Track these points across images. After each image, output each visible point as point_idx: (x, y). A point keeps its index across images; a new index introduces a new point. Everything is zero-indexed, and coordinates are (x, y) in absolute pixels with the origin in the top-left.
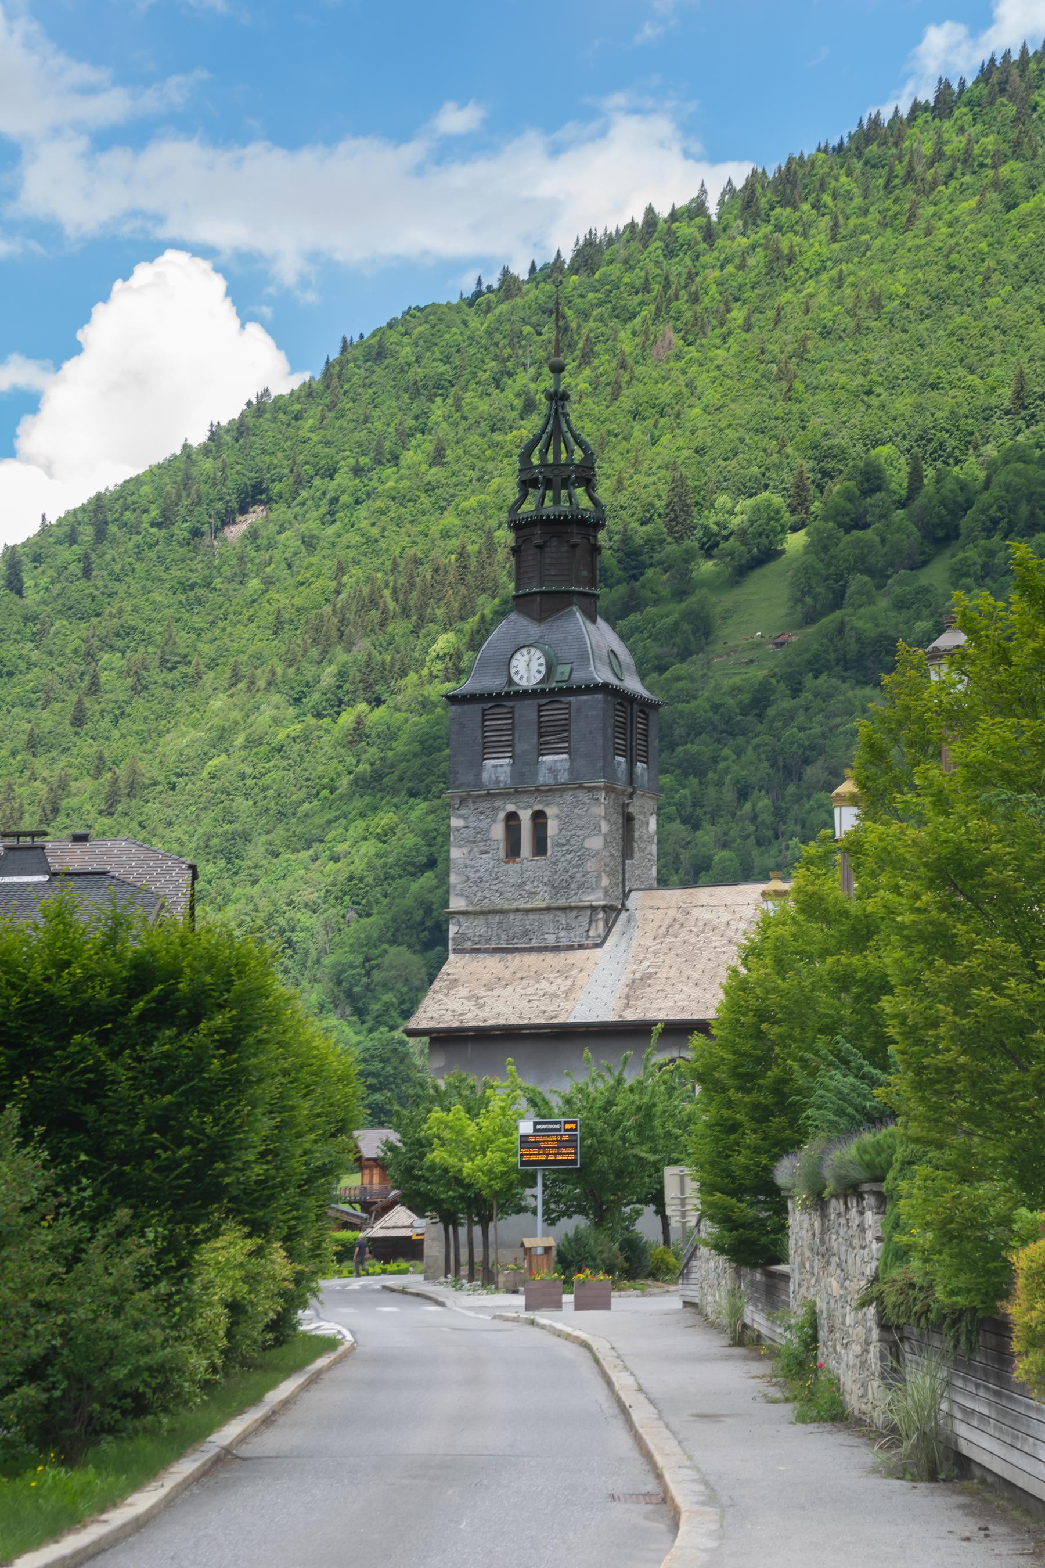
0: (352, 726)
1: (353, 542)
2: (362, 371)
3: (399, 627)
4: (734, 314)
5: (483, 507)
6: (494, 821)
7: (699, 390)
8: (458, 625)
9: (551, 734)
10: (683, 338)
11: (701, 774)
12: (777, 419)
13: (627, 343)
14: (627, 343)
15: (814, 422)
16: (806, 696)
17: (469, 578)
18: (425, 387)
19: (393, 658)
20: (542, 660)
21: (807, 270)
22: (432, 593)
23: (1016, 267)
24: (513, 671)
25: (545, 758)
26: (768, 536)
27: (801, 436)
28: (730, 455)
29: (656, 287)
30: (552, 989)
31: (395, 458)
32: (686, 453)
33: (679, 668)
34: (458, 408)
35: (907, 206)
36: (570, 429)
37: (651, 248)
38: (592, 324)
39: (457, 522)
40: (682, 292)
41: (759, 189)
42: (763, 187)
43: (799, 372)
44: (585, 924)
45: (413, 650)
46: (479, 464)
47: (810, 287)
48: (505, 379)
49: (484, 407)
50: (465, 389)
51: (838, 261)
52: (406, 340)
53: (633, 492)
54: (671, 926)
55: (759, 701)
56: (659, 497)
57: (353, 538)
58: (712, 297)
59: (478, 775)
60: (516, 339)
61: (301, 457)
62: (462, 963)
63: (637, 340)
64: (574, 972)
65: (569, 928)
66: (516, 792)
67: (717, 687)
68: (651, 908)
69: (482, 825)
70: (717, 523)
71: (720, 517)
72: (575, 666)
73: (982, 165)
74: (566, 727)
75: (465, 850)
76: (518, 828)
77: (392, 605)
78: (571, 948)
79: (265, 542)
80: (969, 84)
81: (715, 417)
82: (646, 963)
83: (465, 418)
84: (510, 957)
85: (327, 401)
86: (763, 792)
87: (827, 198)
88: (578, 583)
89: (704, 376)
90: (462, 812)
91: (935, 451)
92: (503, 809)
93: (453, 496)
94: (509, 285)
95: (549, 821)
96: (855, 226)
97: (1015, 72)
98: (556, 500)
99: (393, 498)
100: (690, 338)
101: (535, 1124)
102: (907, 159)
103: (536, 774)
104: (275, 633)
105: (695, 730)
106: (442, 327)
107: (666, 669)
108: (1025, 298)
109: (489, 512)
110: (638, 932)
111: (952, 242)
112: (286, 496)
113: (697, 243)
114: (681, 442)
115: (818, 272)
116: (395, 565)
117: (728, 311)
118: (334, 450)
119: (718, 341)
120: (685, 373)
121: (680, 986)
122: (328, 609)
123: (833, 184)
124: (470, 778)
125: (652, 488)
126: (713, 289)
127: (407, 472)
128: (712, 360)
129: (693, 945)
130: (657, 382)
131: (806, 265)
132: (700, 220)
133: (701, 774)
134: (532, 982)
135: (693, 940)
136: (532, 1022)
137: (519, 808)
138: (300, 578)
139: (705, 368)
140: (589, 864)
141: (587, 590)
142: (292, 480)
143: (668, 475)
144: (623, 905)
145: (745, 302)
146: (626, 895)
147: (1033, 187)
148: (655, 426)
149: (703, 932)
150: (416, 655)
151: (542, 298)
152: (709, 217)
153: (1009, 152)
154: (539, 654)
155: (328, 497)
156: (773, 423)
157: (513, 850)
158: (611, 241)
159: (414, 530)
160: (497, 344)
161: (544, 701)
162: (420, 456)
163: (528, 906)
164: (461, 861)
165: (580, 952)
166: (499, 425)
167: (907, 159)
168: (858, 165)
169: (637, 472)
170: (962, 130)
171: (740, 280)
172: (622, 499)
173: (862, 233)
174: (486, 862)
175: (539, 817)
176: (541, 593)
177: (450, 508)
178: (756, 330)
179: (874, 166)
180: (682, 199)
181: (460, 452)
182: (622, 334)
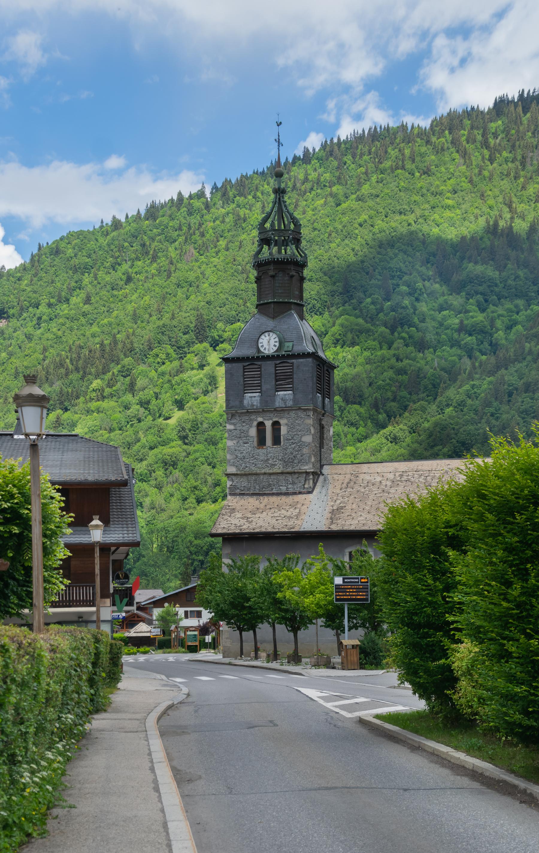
0: (55, 420)
1: (50, 338)
2: (49, 259)
3: (74, 376)
4: (221, 242)
5: (110, 324)
6: (251, 427)
7: (207, 276)
8: (102, 377)
9: (283, 380)
10: (198, 252)
11: (215, 444)
13: (173, 253)
14: (173, 253)
17: (106, 356)
18: (79, 268)
19: (72, 390)
20: (277, 339)
22: (89, 361)
23: (342, 231)
24: (260, 345)
25: (279, 393)
29: (185, 228)
30: (288, 514)
31: (67, 300)
32: (202, 303)
33: (202, 398)
34: (96, 279)
35: (294, 201)
36: (288, 212)
37: (182, 211)
38: (156, 243)
39: (98, 330)
40: (197, 232)
41: (229, 188)
44: (303, 481)
45: (81, 387)
46: (107, 304)
48: (117, 266)
49: (108, 278)
50: (99, 270)
52: (69, 246)
53: (180, 320)
54: (348, 483)
56: (191, 323)
57: (50, 336)
59: (242, 402)
60: (121, 248)
61: (23, 298)
62: (235, 500)
63: (177, 252)
64: (299, 506)
65: (293, 483)
66: (263, 411)
69: (244, 428)
70: (218, 336)
71: (220, 333)
72: (295, 343)
73: (325, 186)
75: (235, 442)
76: (264, 431)
77: (70, 367)
78: (295, 494)
79: (7, 336)
80: (317, 150)
82: (338, 502)
83: (100, 283)
84: (261, 498)
85: (33, 273)
87: (259, 194)
88: (294, 298)
89: (209, 269)
90: (232, 421)
91: (311, 308)
92: (256, 420)
93: (96, 318)
94: (116, 224)
97: (336, 148)
98: (280, 252)
99: (68, 318)
100: (202, 252)
101: (344, 579)
102: (293, 180)
104: (15, 377)
106: (86, 241)
108: (346, 245)
109: (113, 326)
110: (331, 486)
111: (314, 218)
112: (16, 315)
113: (202, 210)
114: (200, 298)
116: (71, 349)
117: (218, 241)
118: (38, 295)
119: (214, 255)
121: (360, 513)
122: (40, 367)
123: (261, 188)
126: (211, 231)
127: (74, 307)
129: (363, 493)
131: (252, 223)
132: (203, 200)
133: (215, 444)
135: (363, 490)
137: (265, 419)
138: (26, 353)
140: (305, 450)
141: (298, 302)
142: (18, 308)
143: (195, 313)
144: (321, 472)
145: (225, 238)
146: (322, 466)
147: (347, 197)
148: (188, 291)
149: (367, 486)
150: (83, 389)
151: (133, 231)
153: (336, 181)
154: (275, 336)
155: (37, 316)
156: (241, 292)
157: (262, 442)
158: (163, 206)
159: (79, 333)
160: (112, 250)
162: (79, 300)
163: (271, 471)
165: (300, 496)
166: (115, 287)
167: (293, 180)
169: (181, 311)
170: (315, 170)
172: (174, 323)
174: (247, 448)
175: (276, 425)
176: (274, 302)
177: (95, 324)
178: (231, 250)
180: (194, 190)
181: (98, 298)
182: (170, 249)
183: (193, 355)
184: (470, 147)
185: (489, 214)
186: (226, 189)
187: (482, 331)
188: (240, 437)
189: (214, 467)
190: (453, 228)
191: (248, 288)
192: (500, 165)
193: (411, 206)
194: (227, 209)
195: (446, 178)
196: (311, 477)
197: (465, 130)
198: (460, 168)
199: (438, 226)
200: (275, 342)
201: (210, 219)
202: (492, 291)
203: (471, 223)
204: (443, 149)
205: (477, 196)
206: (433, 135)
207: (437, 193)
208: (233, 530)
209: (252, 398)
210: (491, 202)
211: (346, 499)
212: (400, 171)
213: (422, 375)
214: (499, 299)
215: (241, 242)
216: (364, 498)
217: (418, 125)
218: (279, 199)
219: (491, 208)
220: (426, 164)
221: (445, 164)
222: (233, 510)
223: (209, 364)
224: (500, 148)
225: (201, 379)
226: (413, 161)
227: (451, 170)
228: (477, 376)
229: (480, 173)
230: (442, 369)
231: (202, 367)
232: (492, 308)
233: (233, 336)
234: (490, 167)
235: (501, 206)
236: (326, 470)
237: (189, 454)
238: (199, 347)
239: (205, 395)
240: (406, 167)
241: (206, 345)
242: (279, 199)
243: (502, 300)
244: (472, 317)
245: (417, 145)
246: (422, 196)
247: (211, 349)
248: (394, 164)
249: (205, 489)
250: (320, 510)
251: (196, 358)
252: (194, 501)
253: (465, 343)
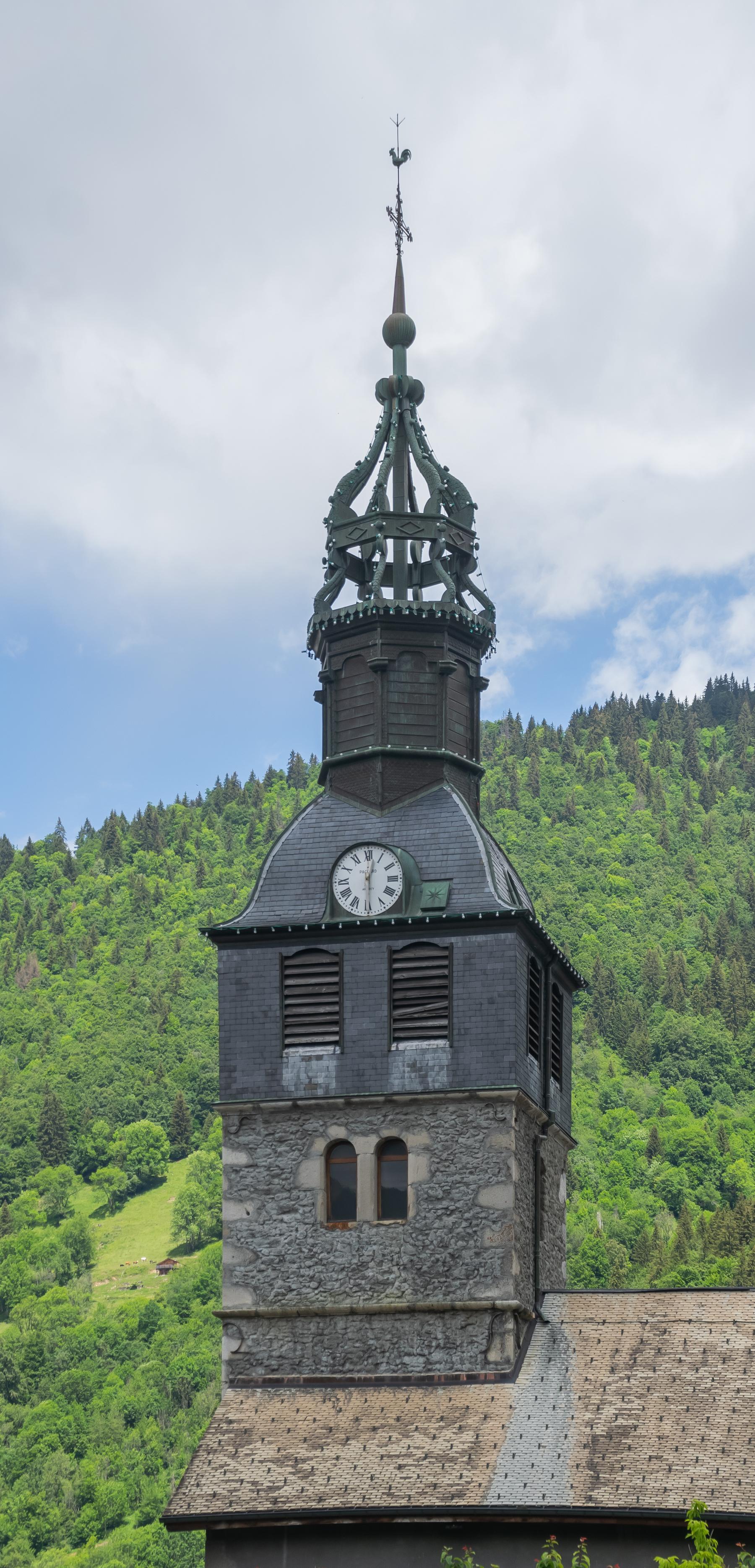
4: (102, 946)
6: (306, 1156)
7: (68, 1017)
9: (419, 1003)
10: (49, 967)
11: (84, 1398)
12: (152, 1049)
15: (191, 1054)
16: (193, 1323)
20: (397, 871)
21: (175, 911)
24: (338, 889)
25: (402, 1046)
26: (148, 1163)
27: (178, 1067)
28: (105, 1081)
29: (16, 916)
30: (439, 1447)
32: (58, 1078)
33: (56, 1291)
41: (119, 832)
42: (123, 830)
43: (174, 1007)
44: (481, 1339)
47: (179, 927)
51: (205, 906)
54: (635, 1352)
55: (148, 1325)
58: (76, 929)
59: (274, 1075)
62: (250, 1403)
65: (449, 1346)
66: (349, 1104)
67: (101, 1310)
68: (591, 1321)
69: (282, 1162)
70: (96, 1149)
71: (100, 1142)
74: (443, 991)
75: (250, 1207)
78: (454, 1381)
81: (89, 1044)
82: (609, 1411)
84: (340, 1394)
86: (151, 1419)
87: (189, 846)
89: (74, 1003)
90: (243, 1139)
92: (323, 1135)
95: (411, 1157)
96: (221, 875)
100: (56, 967)
102: (267, 819)
103: (386, 1073)
105: (80, 1354)
107: (43, 1292)
110: (575, 1361)
113: (57, 877)
114: (52, 1066)
115: (186, 914)
117: (95, 943)
119: (86, 972)
120: (52, 1000)
123: (195, 834)
124: (259, 1079)
125: (23, 1110)
126: (78, 921)
128: (80, 990)
129: (694, 1385)
130: (22, 1008)
132: (59, 855)
133: (84, 1398)
134: (395, 1435)
135: (690, 1376)
136: (414, 1503)
139: (73, 996)
140: (488, 1234)
141: (464, 758)
143: (41, 1098)
145: (112, 936)
146: (539, 1295)
148: (23, 1050)
149: (705, 1363)
152: (69, 852)
154: (388, 858)
156: (149, 1053)
157: (341, 1206)
161: (400, 944)
163: (373, 1304)
164: (244, 1226)
165: (473, 1388)
167: (267, 819)
168: (219, 820)
171: (106, 914)
173: (228, 882)
174: (291, 1228)
175: (391, 1149)
176: (385, 755)
179: (235, 822)
183: (34, 1192)
184: (658, 773)
185: (705, 910)
186: (113, 833)
187: (701, 1157)
188: (268, 1192)
189: (80, 1456)
190: (627, 934)
191: (166, 1044)
192: (726, 815)
193: (535, 884)
194: (116, 876)
195: (608, 831)
196: (510, 1325)
197: (646, 739)
198: (638, 812)
199: (595, 928)
200: (392, 879)
201: (77, 896)
202: (718, 1072)
203: (667, 926)
204: (600, 773)
205: (677, 872)
206: (578, 743)
207: (590, 861)
208: (247, 1501)
209: (310, 1065)
210: (710, 886)
211: (636, 1404)
212: (507, 811)
213: (569, 1246)
214: (736, 1090)
215: (149, 946)
216: (698, 1403)
217: (544, 723)
218: (401, 417)
219: (709, 898)
220: (563, 801)
221: (605, 803)
222: (245, 1436)
223: (72, 1213)
224: (723, 779)
225: (53, 1246)
226: (536, 793)
227: (620, 816)
228: (695, 1254)
229: (682, 827)
230: (613, 1235)
231: (55, 1219)
232: (719, 1108)
233: (131, 1149)
234: (705, 817)
235: (731, 896)
236: (554, 1307)
237: (20, 1425)
238: (51, 1173)
239: (62, 1284)
240: (522, 803)
241: (65, 1168)
242: (401, 417)
243: (742, 1092)
244: (676, 1125)
245: (543, 761)
246: (557, 864)
247: (77, 1179)
248: (494, 796)
249: (56, 1511)
250: (548, 1437)
251: (40, 1201)
252: (27, 1544)
253: (663, 1182)
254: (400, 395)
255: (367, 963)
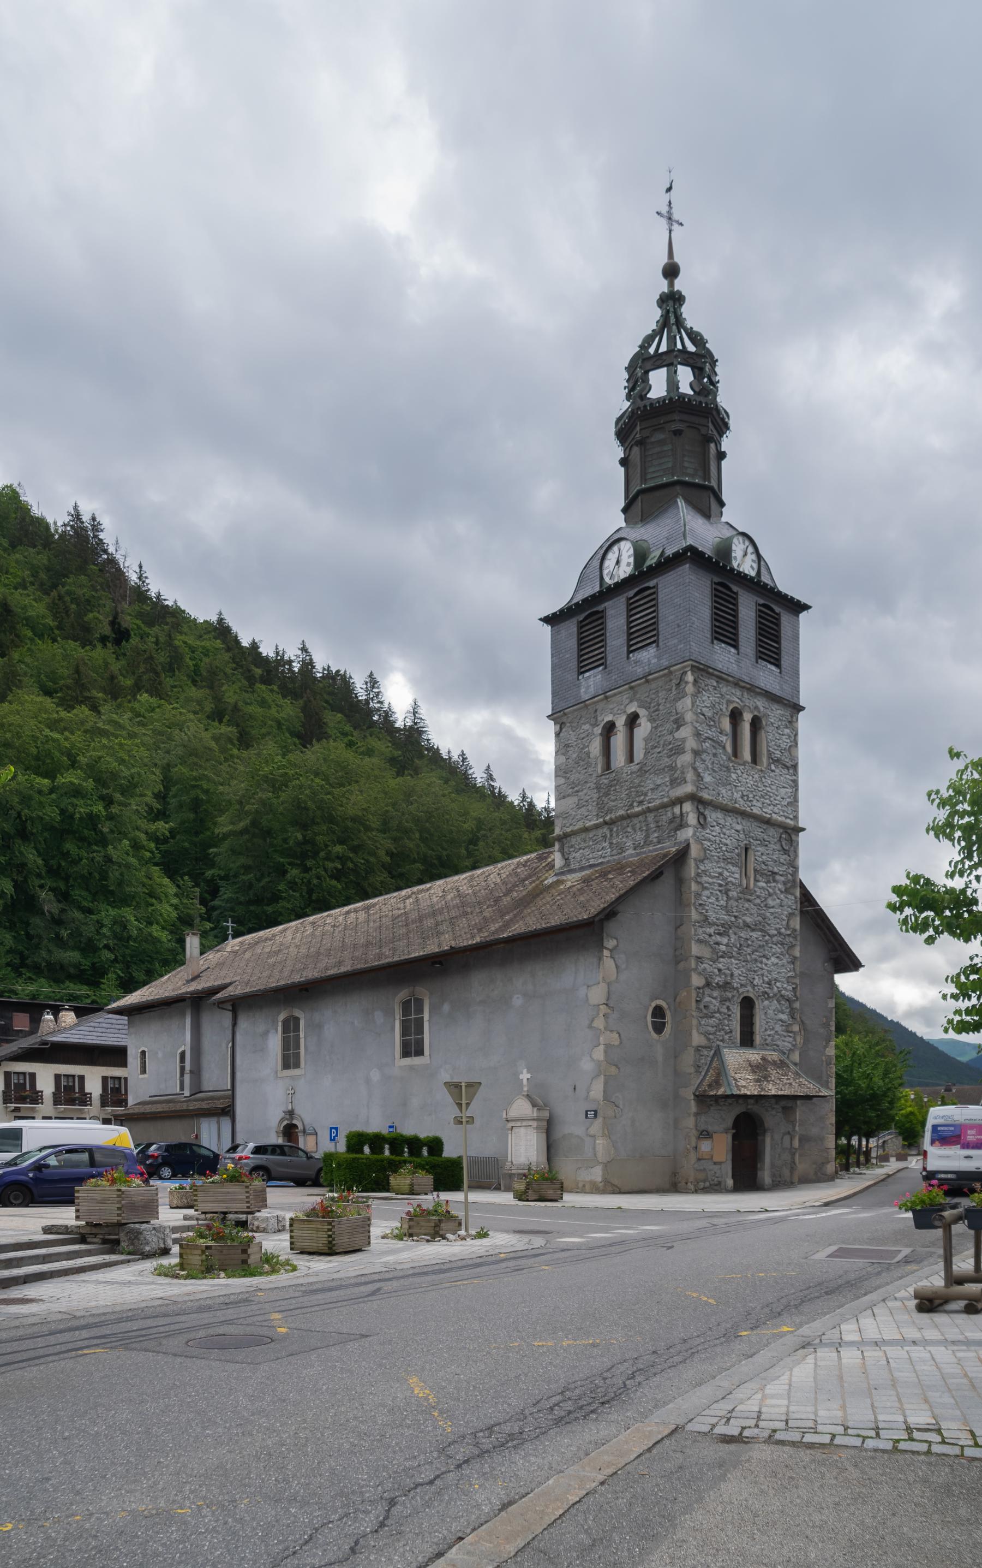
161: (631, 593)
254: (671, 302)
255: (616, 616)
